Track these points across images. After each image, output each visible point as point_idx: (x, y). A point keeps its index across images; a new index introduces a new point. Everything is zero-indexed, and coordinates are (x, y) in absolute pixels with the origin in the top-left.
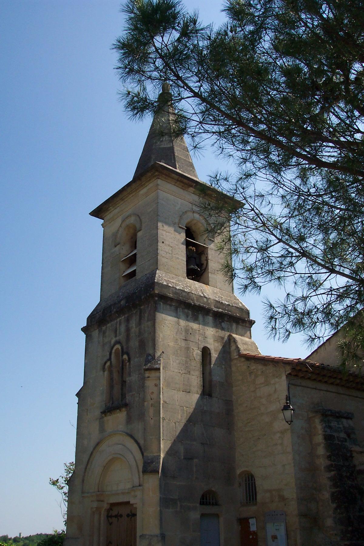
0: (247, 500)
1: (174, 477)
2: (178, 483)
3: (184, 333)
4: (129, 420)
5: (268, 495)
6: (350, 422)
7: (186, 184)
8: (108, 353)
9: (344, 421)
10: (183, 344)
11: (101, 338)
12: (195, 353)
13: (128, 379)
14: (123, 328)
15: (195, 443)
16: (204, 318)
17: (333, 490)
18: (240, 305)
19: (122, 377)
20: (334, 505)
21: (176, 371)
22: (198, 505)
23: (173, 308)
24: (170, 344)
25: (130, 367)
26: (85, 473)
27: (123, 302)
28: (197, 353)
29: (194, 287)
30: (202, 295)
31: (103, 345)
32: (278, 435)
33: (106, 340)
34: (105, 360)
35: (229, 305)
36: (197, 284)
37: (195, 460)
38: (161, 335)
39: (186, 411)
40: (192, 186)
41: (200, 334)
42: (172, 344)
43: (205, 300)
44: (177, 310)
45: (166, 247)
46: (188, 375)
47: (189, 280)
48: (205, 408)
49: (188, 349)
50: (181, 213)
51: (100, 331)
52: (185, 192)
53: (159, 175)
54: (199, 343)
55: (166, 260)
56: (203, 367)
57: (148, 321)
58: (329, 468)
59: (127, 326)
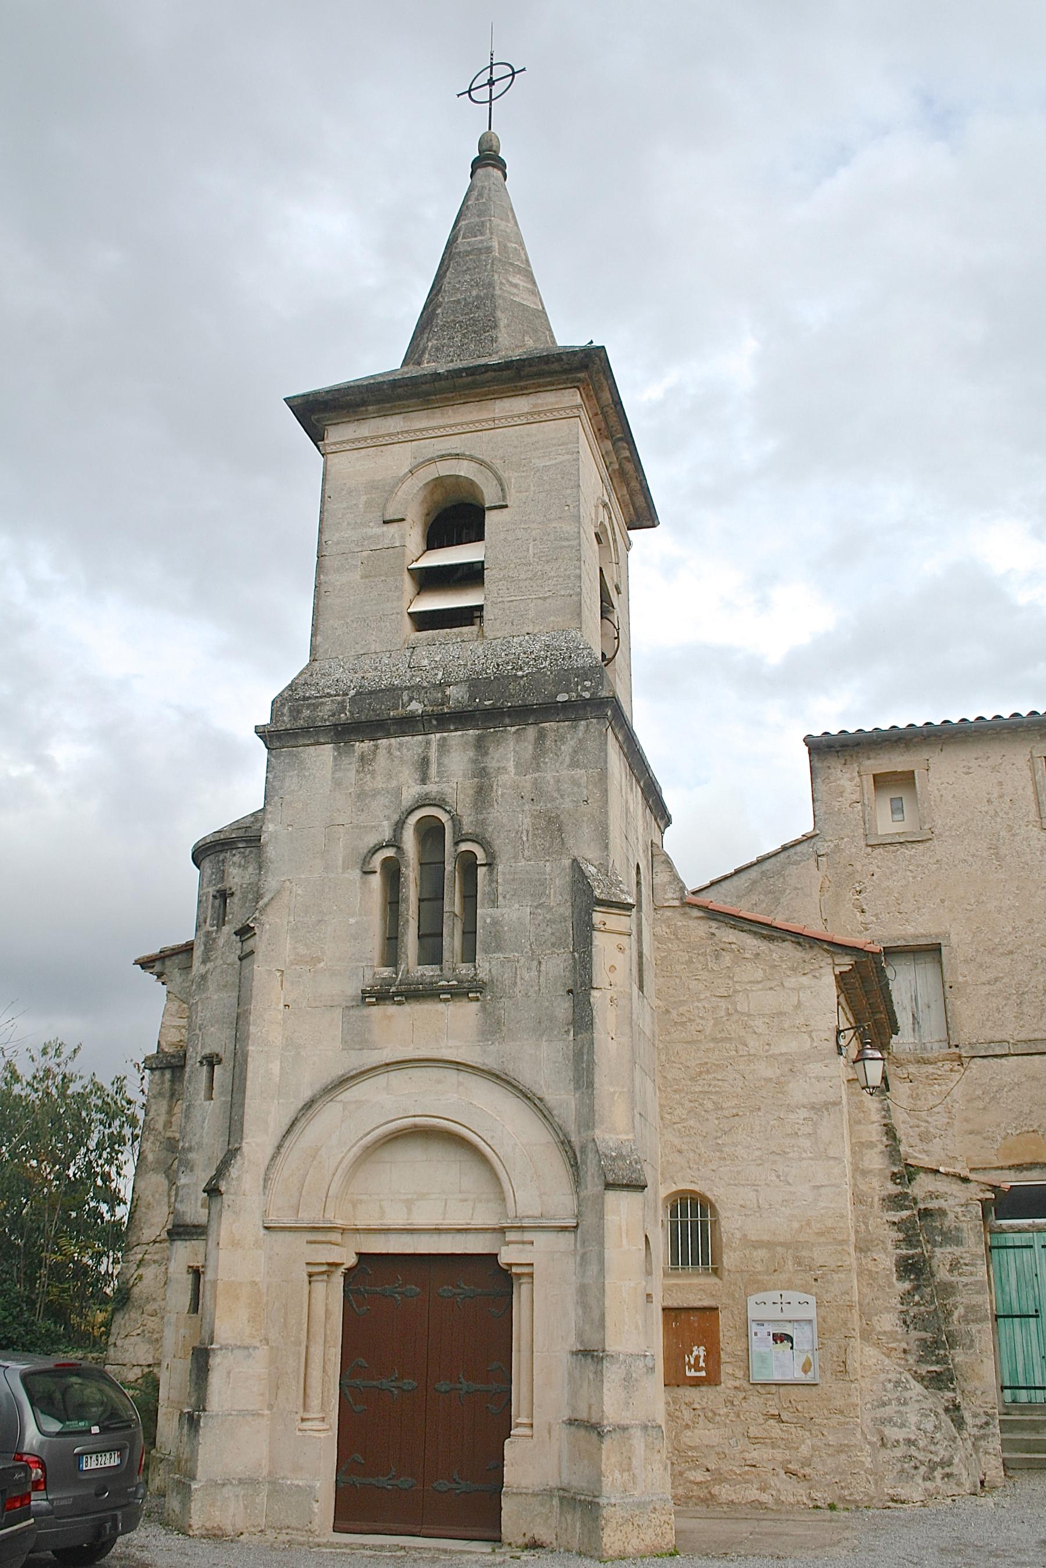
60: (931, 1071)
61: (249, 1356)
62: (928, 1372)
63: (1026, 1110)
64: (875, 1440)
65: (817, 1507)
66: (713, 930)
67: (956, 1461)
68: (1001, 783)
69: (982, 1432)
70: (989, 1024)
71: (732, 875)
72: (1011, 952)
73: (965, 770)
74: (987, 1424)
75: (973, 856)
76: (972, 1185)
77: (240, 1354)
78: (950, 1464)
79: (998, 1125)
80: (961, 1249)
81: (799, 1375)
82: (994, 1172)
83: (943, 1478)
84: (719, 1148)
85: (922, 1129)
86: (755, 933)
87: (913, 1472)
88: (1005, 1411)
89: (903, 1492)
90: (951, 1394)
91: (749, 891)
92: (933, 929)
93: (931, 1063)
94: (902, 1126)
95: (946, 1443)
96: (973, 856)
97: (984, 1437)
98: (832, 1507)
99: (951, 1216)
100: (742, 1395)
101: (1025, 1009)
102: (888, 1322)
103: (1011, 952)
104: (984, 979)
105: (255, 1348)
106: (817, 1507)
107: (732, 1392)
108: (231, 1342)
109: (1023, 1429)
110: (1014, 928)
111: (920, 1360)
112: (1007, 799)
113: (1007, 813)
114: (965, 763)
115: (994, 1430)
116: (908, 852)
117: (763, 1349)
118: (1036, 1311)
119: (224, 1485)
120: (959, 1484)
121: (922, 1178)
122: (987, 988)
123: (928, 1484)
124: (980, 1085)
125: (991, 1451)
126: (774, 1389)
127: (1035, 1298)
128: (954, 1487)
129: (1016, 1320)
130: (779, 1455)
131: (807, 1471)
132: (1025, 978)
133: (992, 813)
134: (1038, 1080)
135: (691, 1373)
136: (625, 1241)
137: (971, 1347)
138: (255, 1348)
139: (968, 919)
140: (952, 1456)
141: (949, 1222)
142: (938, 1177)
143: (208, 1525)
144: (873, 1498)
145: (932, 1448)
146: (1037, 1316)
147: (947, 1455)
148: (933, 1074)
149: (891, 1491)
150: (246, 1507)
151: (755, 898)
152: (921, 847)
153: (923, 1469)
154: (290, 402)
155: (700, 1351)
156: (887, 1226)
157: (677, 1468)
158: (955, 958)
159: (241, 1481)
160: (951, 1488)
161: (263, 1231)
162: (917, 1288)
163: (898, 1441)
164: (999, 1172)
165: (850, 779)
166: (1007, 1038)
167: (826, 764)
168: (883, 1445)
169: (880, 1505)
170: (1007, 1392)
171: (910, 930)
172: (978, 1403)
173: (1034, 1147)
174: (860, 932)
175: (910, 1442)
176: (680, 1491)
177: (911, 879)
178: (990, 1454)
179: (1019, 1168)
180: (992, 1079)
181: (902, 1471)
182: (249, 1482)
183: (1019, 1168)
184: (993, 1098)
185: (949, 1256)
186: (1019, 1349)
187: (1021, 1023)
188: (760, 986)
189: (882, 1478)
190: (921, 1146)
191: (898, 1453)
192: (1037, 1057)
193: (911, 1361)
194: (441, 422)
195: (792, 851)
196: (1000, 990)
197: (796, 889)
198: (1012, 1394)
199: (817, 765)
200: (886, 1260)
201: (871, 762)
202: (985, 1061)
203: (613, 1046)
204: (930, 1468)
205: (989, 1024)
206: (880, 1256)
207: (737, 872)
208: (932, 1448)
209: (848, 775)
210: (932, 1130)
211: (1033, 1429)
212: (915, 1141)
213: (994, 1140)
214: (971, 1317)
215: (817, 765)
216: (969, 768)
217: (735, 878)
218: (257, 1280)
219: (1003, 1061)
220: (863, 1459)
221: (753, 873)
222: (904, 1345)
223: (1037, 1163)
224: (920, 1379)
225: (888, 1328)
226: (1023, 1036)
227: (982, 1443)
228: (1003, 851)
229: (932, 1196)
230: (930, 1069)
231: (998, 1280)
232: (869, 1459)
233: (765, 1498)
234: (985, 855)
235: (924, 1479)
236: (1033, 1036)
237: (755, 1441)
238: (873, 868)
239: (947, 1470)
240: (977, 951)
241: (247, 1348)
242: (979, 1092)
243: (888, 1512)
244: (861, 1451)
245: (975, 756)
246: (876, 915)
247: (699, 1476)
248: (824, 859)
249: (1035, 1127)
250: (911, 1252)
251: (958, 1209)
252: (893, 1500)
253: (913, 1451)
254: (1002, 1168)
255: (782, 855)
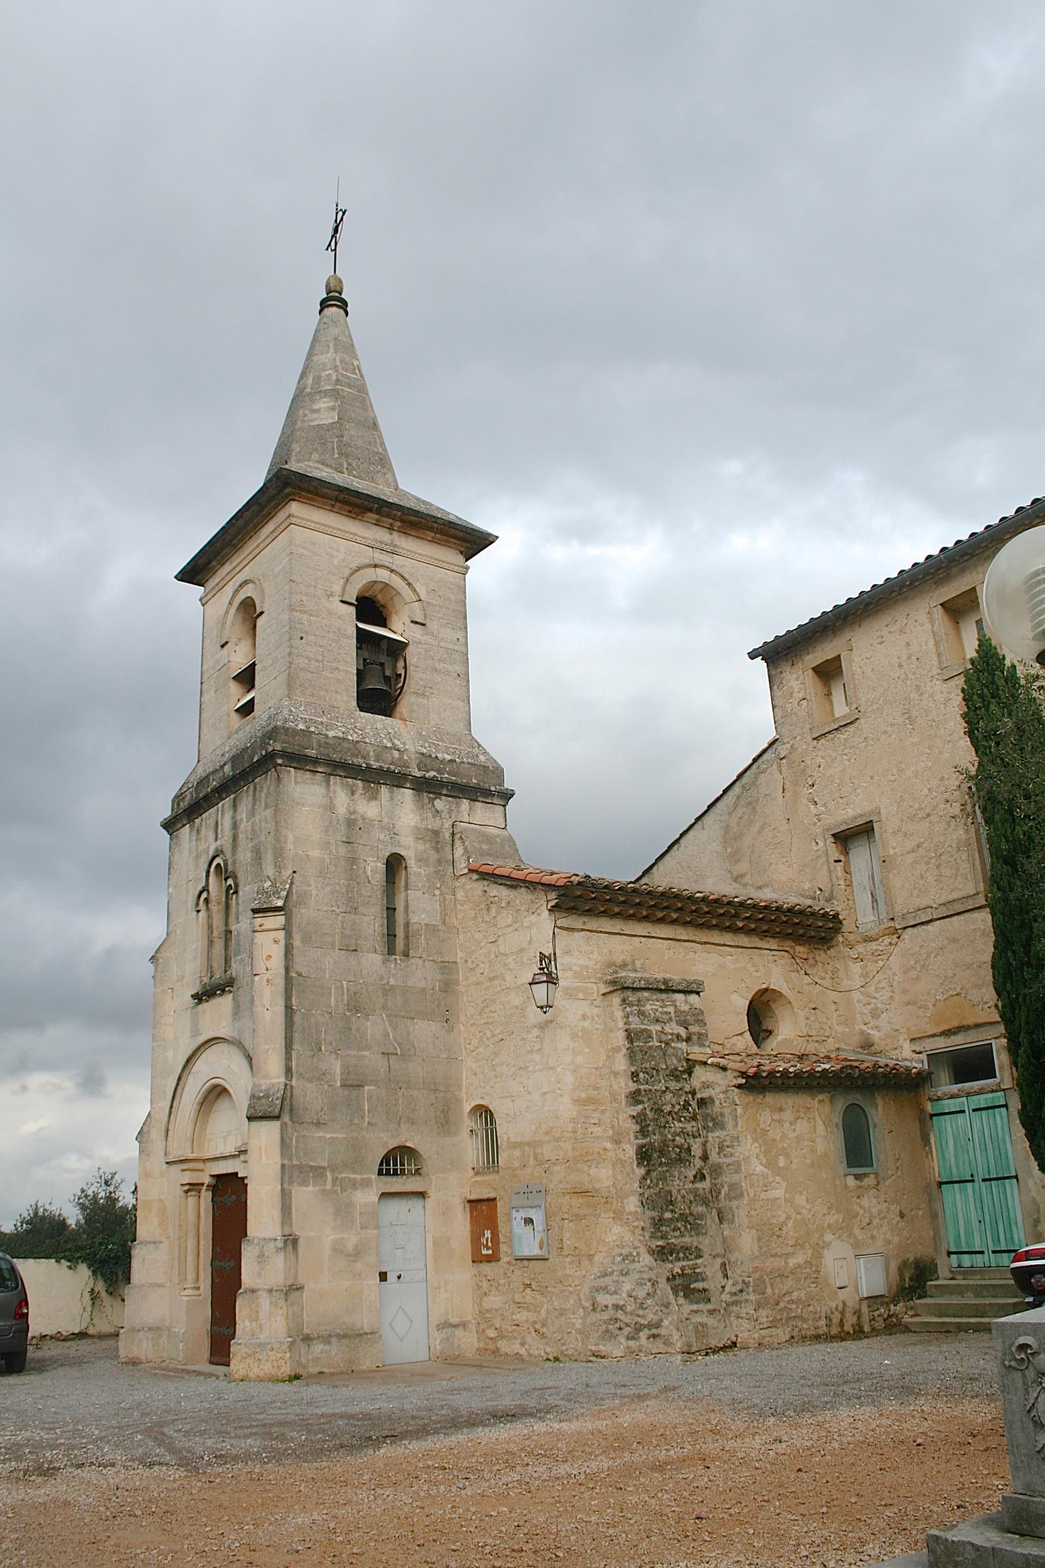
0: (488, 1163)
1: (318, 1124)
2: (328, 1136)
3: (343, 829)
4: (237, 1012)
5: (517, 1153)
6: (693, 998)
7: (357, 506)
8: (204, 874)
9: (679, 997)
10: (343, 850)
11: (194, 843)
12: (369, 869)
13: (233, 928)
14: (226, 823)
15: (366, 1053)
16: (392, 792)
17: (639, 1141)
18: (482, 758)
19: (227, 924)
20: (642, 1171)
21: (326, 908)
22: (374, 1176)
23: (319, 776)
24: (311, 853)
25: (238, 904)
26: (170, 1115)
27: (227, 768)
28: (375, 868)
29: (373, 726)
30: (389, 745)
31: (198, 857)
32: (536, 1032)
33: (202, 847)
34: (200, 888)
35: (452, 761)
36: (380, 720)
37: (366, 1088)
38: (291, 836)
39: (348, 990)
40: (370, 510)
41: (382, 828)
42: (315, 853)
43: (396, 754)
44: (328, 782)
45: (309, 648)
46: (353, 916)
47: (362, 714)
48: (392, 982)
49: (352, 861)
50: (347, 572)
51: (191, 828)
52: (357, 523)
53: (294, 494)
54: (380, 846)
55: (309, 676)
56: (387, 897)
57: (266, 807)
58: (876, 1065)
59: (233, 817)
60: (875, 947)
61: (157, 1248)
62: (657, 1246)
63: (950, 973)
64: (588, 1305)
65: (548, 1359)
66: (486, 888)
67: (666, 1323)
68: (908, 644)
69: (734, 1298)
70: (916, 892)
71: (721, 796)
72: (929, 815)
73: (880, 640)
74: (741, 1291)
75: (892, 725)
76: (729, 1072)
77: (151, 1247)
78: (658, 1325)
79: (929, 993)
80: (725, 1133)
81: (536, 1251)
82: (927, 1041)
83: (648, 1338)
84: (493, 1068)
85: (872, 1005)
86: (506, 885)
87: (617, 1332)
88: (951, 1276)
89: (603, 1349)
90: (670, 1266)
91: (736, 805)
92: (867, 807)
93: (875, 940)
94: (857, 1005)
95: (657, 1308)
96: (892, 725)
97: (735, 1303)
98: (556, 1359)
99: (717, 1102)
100: (511, 1268)
101: (943, 870)
102: (632, 1204)
103: (929, 815)
104: (909, 848)
105: (161, 1242)
106: (548, 1359)
107: (506, 1266)
108: (148, 1239)
109: (951, 1294)
110: (929, 790)
111: (653, 1236)
112: (914, 658)
113: (914, 673)
114: (878, 634)
115: (747, 1297)
116: (841, 736)
117: (521, 1231)
118: (972, 1176)
119: (330, 1336)
120: (668, 1343)
121: (698, 1070)
122: (912, 855)
123: (631, 1343)
124: (913, 955)
125: (744, 1315)
126: (526, 1263)
127: (970, 1162)
128: (662, 1346)
129: (956, 1185)
130: (532, 1316)
131: (545, 1330)
132: (942, 839)
133: (903, 676)
134: (958, 940)
135: (485, 1252)
136: (264, 1158)
137: (733, 1221)
138: (161, 1242)
139: (893, 790)
140: (662, 1320)
141: (716, 1108)
142: (708, 1068)
143: (130, 1356)
144: (580, 1353)
145: (641, 1312)
146: (973, 1181)
147: (656, 1318)
148: (877, 950)
149: (594, 1348)
150: (154, 1346)
151: (740, 811)
152: (851, 729)
153: (627, 1330)
154: (176, 577)
155: (488, 1234)
156: (629, 1120)
157: (482, 1327)
158: (885, 832)
159: (150, 1329)
160: (658, 1346)
161: (165, 1166)
162: (648, 1173)
163: (606, 1307)
164: (932, 1039)
165: (799, 678)
166: (931, 903)
167: (779, 670)
168: (594, 1309)
169: (584, 1359)
170: (953, 1256)
171: (851, 812)
172: (739, 1272)
173: (959, 1011)
174: (815, 824)
175: (617, 1307)
176: (482, 1345)
177: (847, 763)
178: (742, 1318)
179: (947, 1033)
180: (921, 947)
181: (607, 1331)
182: (155, 1329)
183: (947, 1033)
184: (923, 966)
185: (717, 1140)
186: (960, 1214)
187: (941, 886)
188: (510, 929)
189: (587, 1337)
190: (873, 1022)
191: (605, 1316)
192: (956, 917)
193: (647, 1238)
194: (237, 562)
195: (760, 760)
196: (922, 856)
197: (766, 795)
198: (958, 1259)
199: (773, 673)
200: (630, 1151)
201: (811, 656)
202: (915, 930)
203: (268, 1015)
204: (636, 1329)
205: (916, 892)
206: (627, 1147)
207: (725, 791)
208: (641, 1312)
209: (795, 676)
210: (879, 1006)
211: (959, 1294)
212: (868, 1018)
213: (926, 1008)
214: (732, 1195)
215: (773, 673)
216: (882, 637)
217: (725, 797)
218: (163, 1197)
219: (929, 927)
220: (574, 1321)
221: (737, 789)
222: (642, 1224)
223: (963, 1027)
224: (651, 1252)
225: (633, 1209)
226: (942, 900)
227: (734, 1308)
228: (914, 714)
229: (706, 1085)
230: (873, 946)
231: (939, 1146)
232: (580, 1321)
233: (523, 1351)
234: (900, 721)
235: (628, 1338)
236: (951, 898)
237: (519, 1305)
238: (819, 760)
239: (654, 1331)
240: (902, 820)
241: (154, 1243)
242: (912, 962)
243: (590, 1364)
244: (574, 1314)
245: (885, 623)
246: (824, 805)
247: (492, 1333)
248: (784, 761)
249: (958, 990)
250: (644, 1141)
251: (721, 1096)
252: (594, 1355)
253: (619, 1314)
254: (933, 1036)
255: (754, 767)
